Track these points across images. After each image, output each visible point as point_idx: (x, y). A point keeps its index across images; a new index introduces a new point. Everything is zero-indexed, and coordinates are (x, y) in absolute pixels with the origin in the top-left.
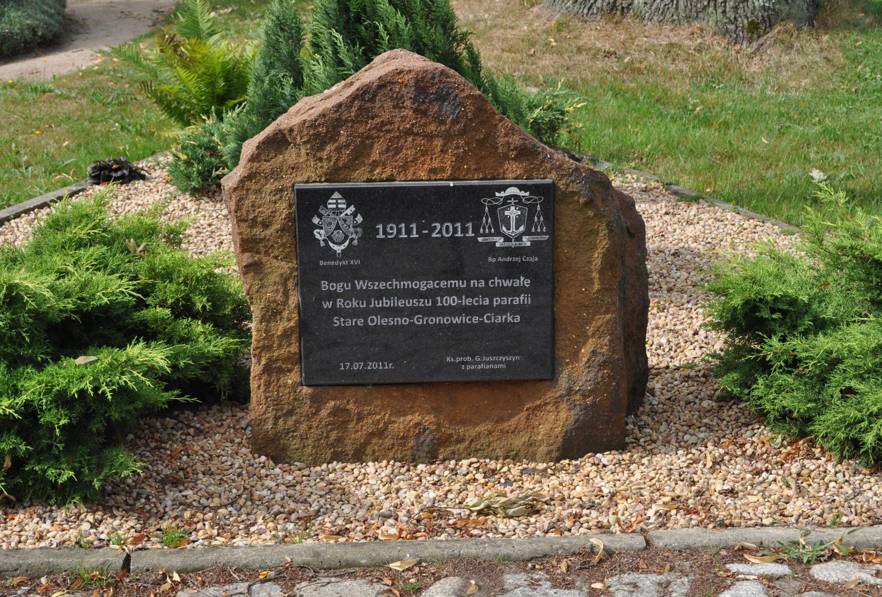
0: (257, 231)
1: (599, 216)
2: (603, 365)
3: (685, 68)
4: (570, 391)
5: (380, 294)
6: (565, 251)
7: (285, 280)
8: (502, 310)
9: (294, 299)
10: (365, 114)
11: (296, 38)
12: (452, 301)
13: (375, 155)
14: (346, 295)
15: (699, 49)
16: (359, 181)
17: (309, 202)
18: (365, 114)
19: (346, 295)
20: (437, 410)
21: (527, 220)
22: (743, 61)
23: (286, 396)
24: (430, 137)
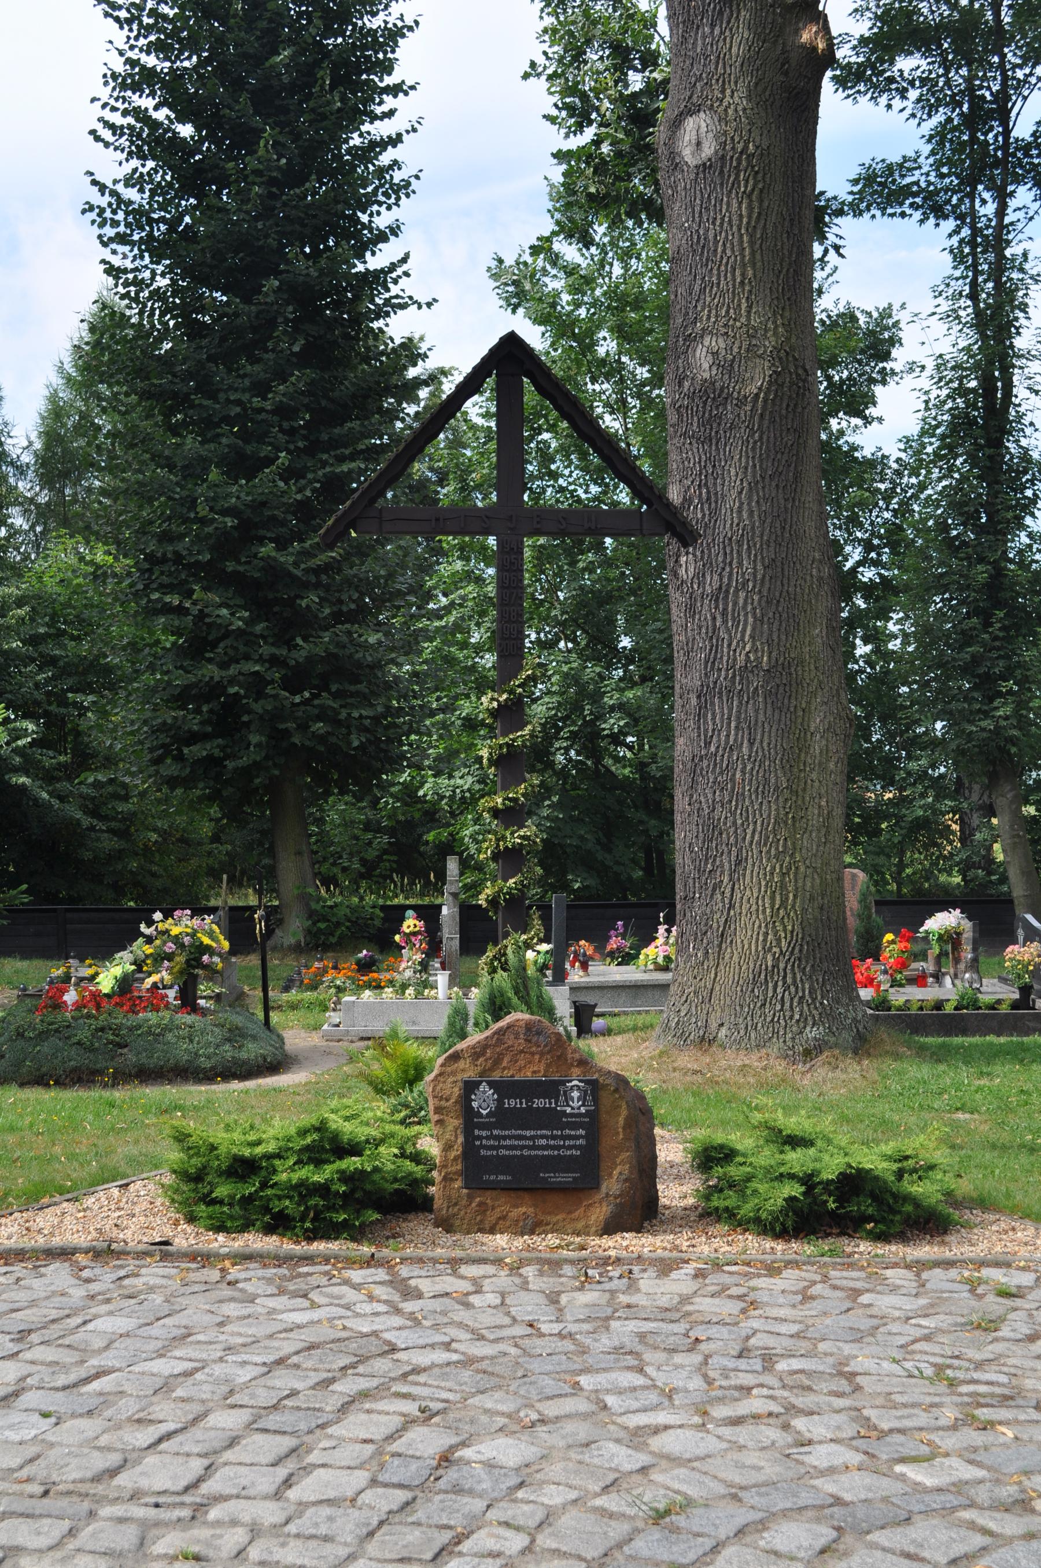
0: (443, 1103)
1: (621, 1097)
2: (626, 1180)
3: (752, 1080)
4: (607, 1195)
5: (505, 1138)
6: (604, 1116)
7: (456, 1129)
8: (570, 1147)
9: (461, 1139)
10: (500, 1042)
11: (465, 1018)
12: (543, 1142)
13: (505, 1064)
14: (487, 1138)
15: (765, 1069)
16: (496, 1076)
17: (470, 1087)
18: (500, 1042)
19: (487, 1138)
20: (535, 1206)
21: (583, 1098)
22: (798, 1077)
23: (454, 1195)
24: (533, 1054)
